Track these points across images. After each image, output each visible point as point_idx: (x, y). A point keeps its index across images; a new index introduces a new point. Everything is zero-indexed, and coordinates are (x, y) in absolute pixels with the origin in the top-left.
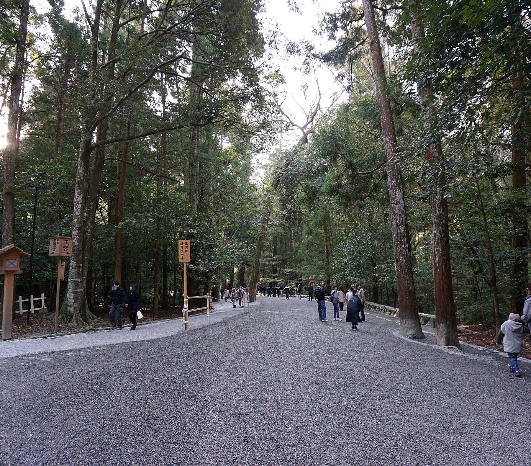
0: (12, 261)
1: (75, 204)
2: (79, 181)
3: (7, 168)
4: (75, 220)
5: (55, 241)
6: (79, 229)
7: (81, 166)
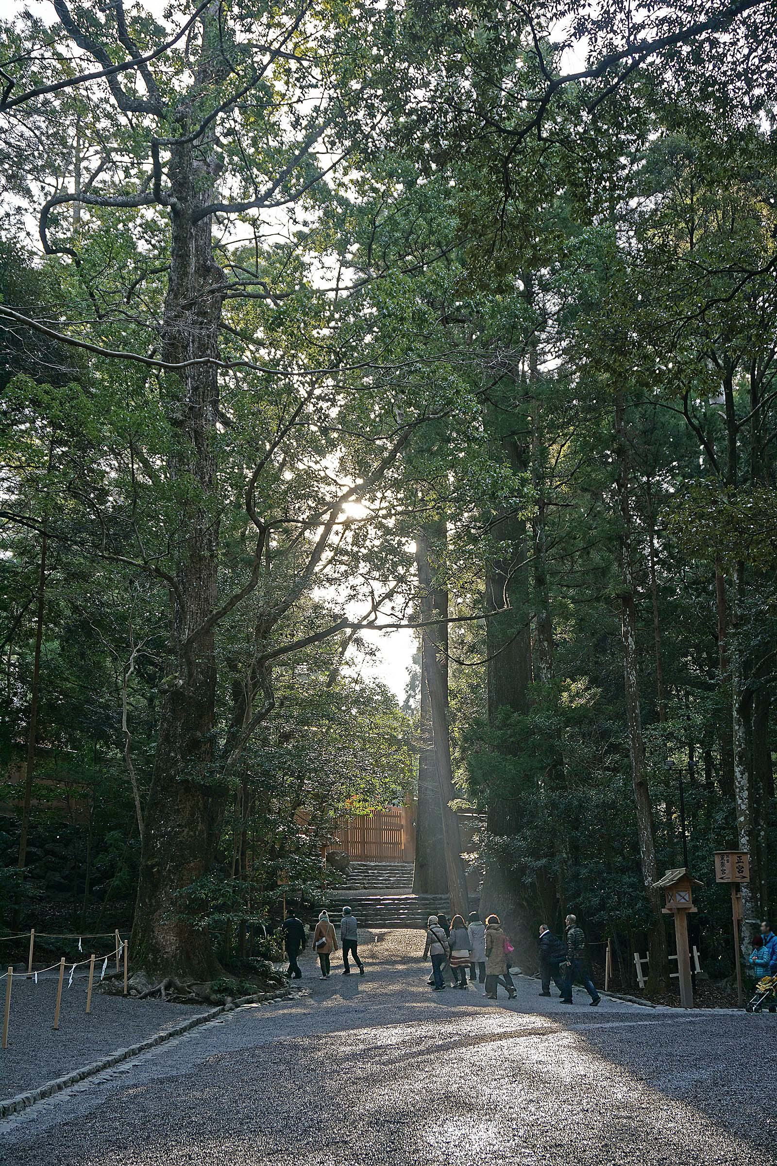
0: (683, 894)
1: (738, 790)
2: (739, 752)
3: (634, 744)
4: (742, 819)
5: (722, 859)
6: (750, 833)
7: (739, 725)
